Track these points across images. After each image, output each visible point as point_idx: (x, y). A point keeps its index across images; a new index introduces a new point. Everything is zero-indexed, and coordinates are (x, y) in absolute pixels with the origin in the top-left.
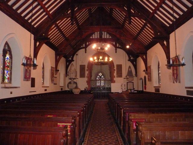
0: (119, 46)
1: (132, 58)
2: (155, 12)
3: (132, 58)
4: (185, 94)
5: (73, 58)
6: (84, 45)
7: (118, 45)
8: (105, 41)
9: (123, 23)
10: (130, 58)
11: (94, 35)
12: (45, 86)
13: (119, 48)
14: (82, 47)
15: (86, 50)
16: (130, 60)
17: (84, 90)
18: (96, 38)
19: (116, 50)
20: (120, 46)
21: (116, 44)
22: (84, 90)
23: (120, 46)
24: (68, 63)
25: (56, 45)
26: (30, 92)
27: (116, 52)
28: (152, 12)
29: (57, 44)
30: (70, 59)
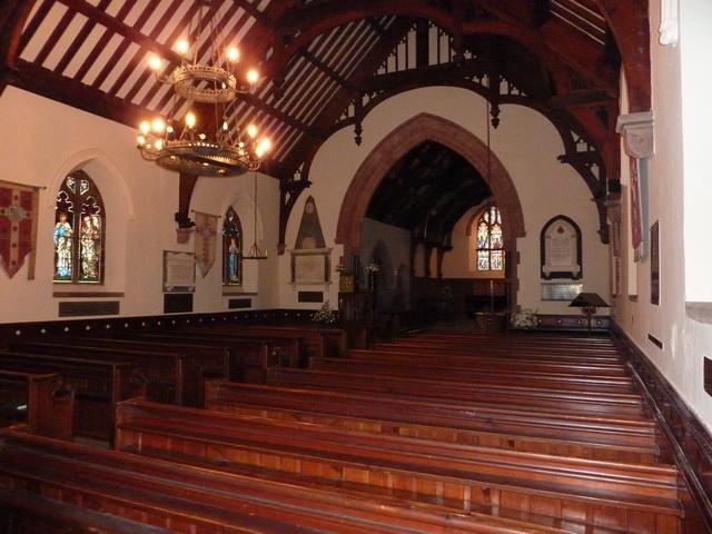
0: (510, 89)
1: (582, 147)
2: (309, 57)
3: (582, 147)
4: (51, 314)
5: (305, 174)
6: (352, 111)
7: (504, 88)
8: (237, 146)
9: (314, 65)
10: (570, 145)
11: (391, 60)
12: (245, 291)
13: (510, 99)
14: (343, 117)
15: (358, 131)
16: (570, 157)
17: (157, 309)
18: (400, 69)
19: (495, 112)
20: (515, 92)
21: (495, 85)
22: (157, 309)
23: (515, 92)
24: (288, 196)
25: (345, 74)
26: (651, 338)
27: (496, 123)
28: (310, 50)
29: (348, 70)
30: (297, 177)
